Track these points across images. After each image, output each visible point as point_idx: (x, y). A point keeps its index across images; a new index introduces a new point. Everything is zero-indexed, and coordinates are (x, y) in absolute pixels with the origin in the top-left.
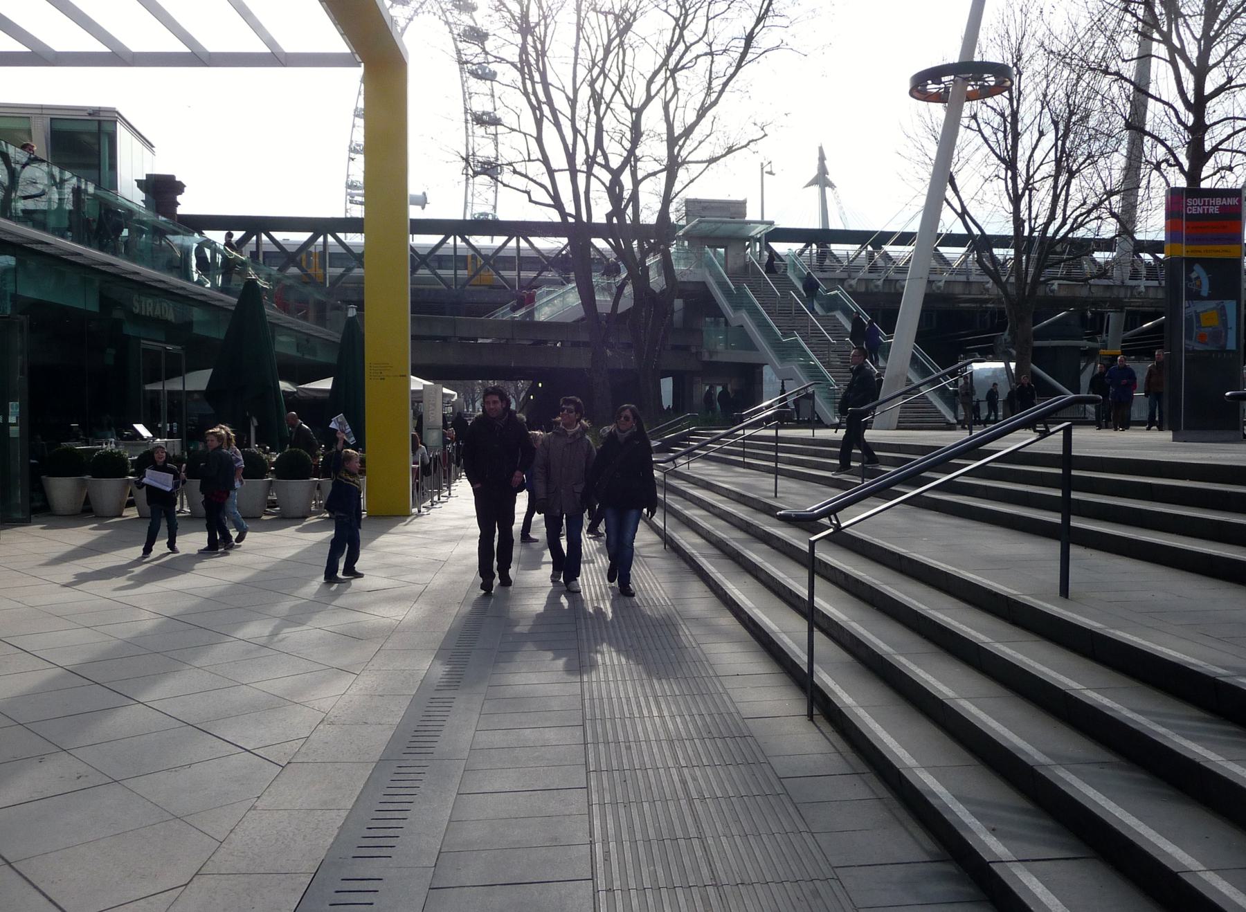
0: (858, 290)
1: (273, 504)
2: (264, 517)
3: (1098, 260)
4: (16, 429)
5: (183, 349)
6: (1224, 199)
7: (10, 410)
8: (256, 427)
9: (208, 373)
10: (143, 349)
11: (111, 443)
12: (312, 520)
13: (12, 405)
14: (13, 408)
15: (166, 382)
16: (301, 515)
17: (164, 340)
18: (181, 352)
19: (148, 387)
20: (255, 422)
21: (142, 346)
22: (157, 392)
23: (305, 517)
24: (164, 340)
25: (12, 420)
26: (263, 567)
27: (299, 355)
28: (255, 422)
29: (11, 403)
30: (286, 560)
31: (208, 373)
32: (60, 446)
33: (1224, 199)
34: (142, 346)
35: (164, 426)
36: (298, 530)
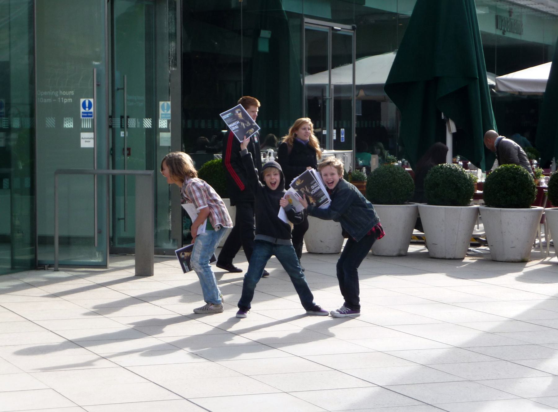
0: (281, 200)
1: (477, 242)
2: (467, 260)
3: (427, 250)
4: (168, 135)
5: (353, 29)
6: (317, 190)
7: (161, 112)
8: (454, 135)
9: (389, 58)
10: (307, 30)
11: (270, 155)
12: (533, 265)
13: (163, 105)
14: (163, 110)
15: (333, 71)
16: (519, 258)
17: (329, 17)
18: (351, 33)
19: (310, 80)
20: (452, 127)
21: (306, 26)
22: (321, 88)
23: (523, 261)
24: (329, 17)
25: (163, 124)
26: (487, 327)
27: (499, 33)
28: (452, 127)
29: (161, 103)
30: (514, 320)
31: (389, 58)
32: (213, 158)
33: (317, 190)
34: (306, 26)
35: (330, 133)
36: (519, 279)
